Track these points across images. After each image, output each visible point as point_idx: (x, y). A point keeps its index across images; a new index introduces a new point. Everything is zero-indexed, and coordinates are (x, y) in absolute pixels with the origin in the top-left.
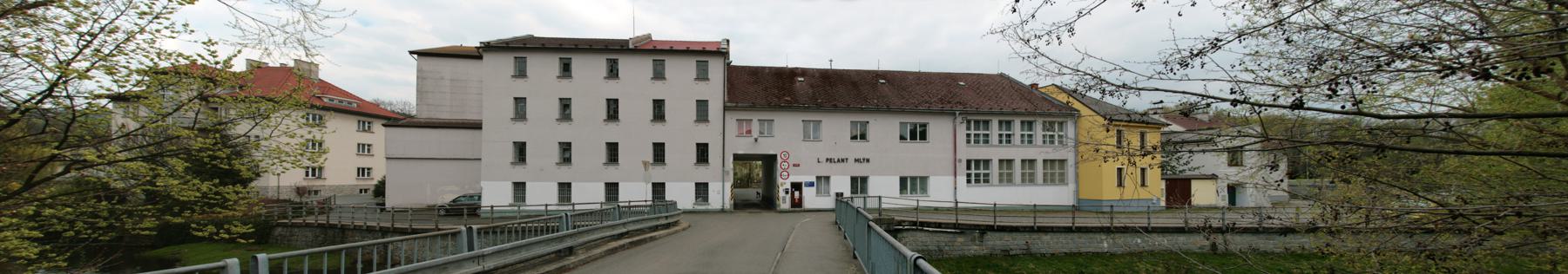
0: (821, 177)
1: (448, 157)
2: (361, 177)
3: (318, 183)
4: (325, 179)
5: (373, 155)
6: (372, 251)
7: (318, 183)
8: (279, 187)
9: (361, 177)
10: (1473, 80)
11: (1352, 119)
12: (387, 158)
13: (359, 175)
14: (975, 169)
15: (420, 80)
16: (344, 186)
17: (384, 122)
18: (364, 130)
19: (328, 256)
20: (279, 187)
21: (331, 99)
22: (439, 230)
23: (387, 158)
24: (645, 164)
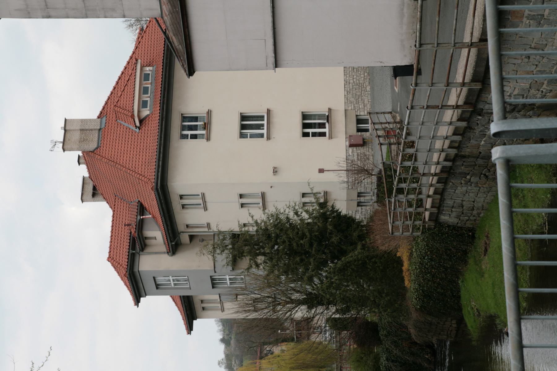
0: (241, 133)
1: (270, 19)
2: (326, 130)
3: (339, 120)
4: (330, 110)
5: (269, 111)
6: (522, 214)
7: (339, 120)
8: (347, 170)
9: (326, 130)
10: (501, 346)
11: (445, 366)
12: (276, 65)
13: (323, 134)
14: (368, 123)
15: (52, 13)
16: (346, 83)
17: (180, 71)
18: (207, 126)
19: (505, 27)
20: (347, 170)
21: (144, 104)
22: (483, 39)
23: (276, 65)
24: (231, 271)
